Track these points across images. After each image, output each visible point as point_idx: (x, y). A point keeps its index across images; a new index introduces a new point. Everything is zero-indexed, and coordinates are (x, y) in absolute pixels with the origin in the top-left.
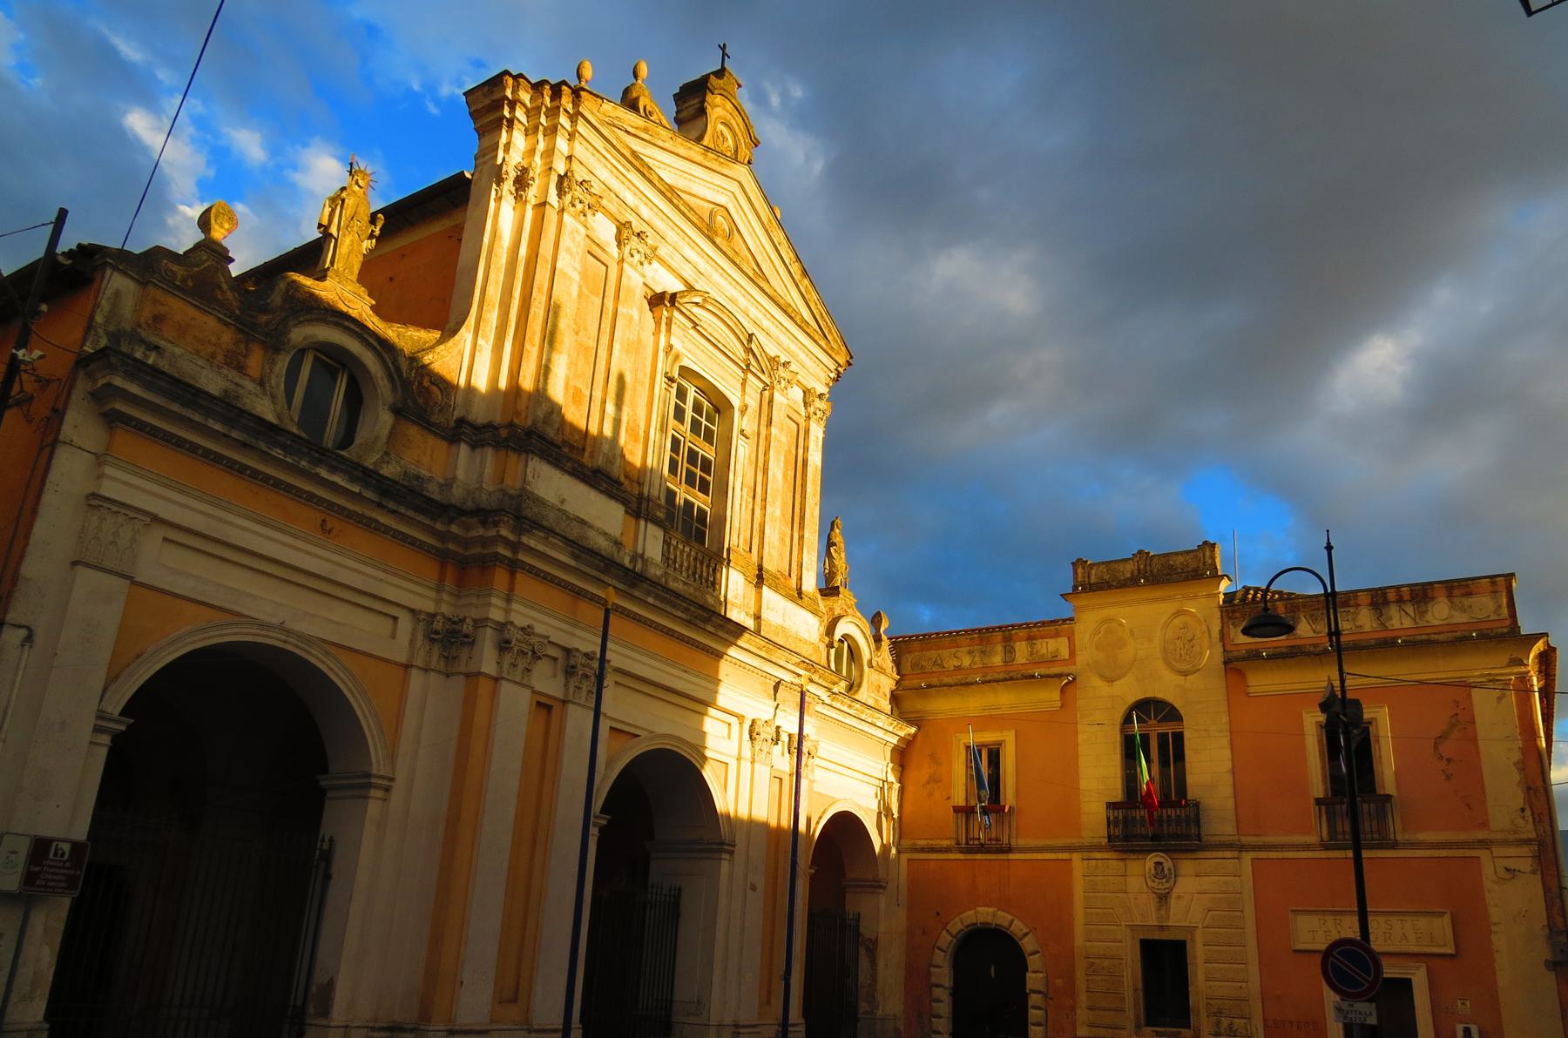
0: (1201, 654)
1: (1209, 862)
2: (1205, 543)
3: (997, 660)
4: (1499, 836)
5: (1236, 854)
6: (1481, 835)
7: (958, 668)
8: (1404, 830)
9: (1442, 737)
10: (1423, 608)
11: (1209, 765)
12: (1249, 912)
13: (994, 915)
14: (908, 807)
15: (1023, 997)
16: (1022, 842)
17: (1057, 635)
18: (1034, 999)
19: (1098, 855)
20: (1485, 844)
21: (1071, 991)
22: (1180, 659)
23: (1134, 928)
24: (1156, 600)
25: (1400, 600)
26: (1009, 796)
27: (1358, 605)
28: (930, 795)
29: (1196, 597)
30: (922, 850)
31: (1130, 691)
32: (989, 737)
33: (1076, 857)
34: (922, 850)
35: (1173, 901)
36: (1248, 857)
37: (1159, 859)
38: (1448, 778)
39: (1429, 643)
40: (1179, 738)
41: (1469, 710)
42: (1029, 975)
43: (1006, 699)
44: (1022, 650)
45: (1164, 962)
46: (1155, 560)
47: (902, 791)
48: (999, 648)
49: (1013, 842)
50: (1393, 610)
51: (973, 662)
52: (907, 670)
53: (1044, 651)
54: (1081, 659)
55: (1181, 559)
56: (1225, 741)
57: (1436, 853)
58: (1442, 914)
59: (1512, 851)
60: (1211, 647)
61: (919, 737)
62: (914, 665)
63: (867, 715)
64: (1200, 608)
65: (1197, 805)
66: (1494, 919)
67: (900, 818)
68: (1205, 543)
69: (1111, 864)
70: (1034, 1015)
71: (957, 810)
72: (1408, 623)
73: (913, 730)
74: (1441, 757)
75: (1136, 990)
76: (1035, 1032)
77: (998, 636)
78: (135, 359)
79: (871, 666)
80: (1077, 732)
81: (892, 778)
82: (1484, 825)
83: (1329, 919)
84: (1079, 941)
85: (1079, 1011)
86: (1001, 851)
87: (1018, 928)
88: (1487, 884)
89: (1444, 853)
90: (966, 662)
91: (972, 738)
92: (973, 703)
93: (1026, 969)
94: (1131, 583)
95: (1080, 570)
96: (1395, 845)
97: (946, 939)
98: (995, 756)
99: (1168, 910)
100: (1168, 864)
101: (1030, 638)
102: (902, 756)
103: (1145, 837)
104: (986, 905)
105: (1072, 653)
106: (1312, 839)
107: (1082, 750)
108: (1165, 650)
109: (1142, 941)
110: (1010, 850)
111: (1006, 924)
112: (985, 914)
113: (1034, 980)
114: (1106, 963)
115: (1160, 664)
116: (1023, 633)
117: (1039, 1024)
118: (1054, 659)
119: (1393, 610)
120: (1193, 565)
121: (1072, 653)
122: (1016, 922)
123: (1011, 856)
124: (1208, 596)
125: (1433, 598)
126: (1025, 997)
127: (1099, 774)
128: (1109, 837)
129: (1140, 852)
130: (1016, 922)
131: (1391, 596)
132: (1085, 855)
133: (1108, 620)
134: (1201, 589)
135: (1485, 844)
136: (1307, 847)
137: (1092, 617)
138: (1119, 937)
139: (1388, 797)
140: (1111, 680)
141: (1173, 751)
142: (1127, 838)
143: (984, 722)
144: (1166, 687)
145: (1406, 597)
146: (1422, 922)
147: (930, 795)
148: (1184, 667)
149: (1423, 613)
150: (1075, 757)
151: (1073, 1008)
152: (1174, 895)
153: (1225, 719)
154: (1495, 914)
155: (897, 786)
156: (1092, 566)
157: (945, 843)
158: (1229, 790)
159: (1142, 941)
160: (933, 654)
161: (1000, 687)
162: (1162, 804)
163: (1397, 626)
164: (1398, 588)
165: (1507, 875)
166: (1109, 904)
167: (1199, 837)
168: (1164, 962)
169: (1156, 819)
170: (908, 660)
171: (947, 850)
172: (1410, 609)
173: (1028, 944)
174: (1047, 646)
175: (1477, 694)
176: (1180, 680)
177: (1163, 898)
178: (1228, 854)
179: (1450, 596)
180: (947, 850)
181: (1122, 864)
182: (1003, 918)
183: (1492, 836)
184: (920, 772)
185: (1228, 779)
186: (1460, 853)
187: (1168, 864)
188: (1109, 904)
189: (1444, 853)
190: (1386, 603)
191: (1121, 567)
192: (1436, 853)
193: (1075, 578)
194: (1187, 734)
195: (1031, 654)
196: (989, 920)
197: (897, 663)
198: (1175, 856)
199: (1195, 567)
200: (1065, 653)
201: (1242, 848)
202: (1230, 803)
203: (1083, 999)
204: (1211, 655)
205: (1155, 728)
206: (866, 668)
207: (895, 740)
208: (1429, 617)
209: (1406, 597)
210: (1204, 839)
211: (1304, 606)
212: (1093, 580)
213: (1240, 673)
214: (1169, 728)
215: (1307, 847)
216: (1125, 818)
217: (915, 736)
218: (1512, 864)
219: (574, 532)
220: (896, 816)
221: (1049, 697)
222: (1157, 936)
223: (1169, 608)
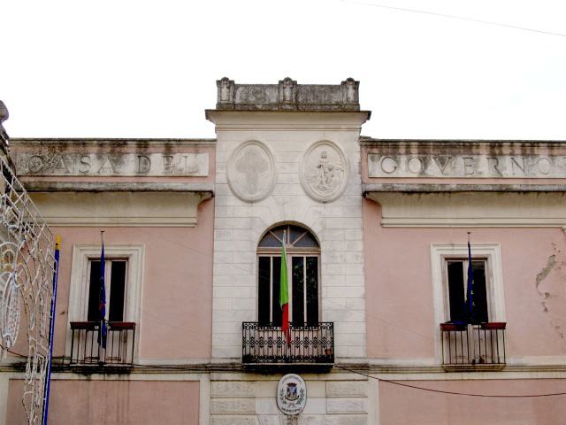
2: (350, 80)
11: (341, 292)
39: (509, 191)
40: (314, 264)
44: (157, 161)
53: (182, 165)
74: (541, 294)
77: (132, 148)
78: (488, 329)
80: (366, 321)
121: (213, 171)
134: (346, 123)
185: (361, 304)
186: (554, 375)
194: (324, 260)
199: (337, 104)
205: (287, 250)
214: (305, 252)
219: (472, 189)
223: (315, 136)
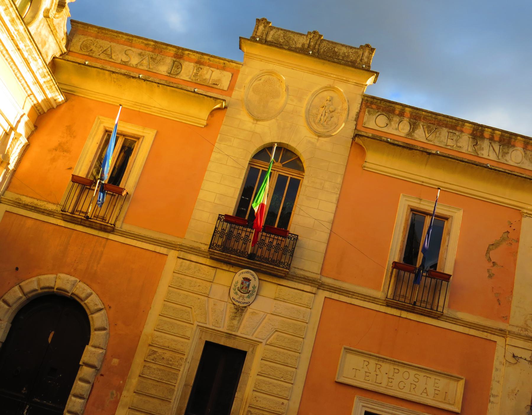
0: (337, 125)
1: (288, 290)
3: (163, 69)
4: (515, 330)
5: (314, 290)
6: (501, 325)
7: (125, 64)
8: (449, 307)
9: (494, 246)
10: (506, 150)
11: (314, 213)
12: (311, 336)
13: (74, 285)
14: (26, 164)
15: (278, 236)
16: (126, 227)
17: (224, 68)
18: (85, 372)
19: (194, 258)
20: (502, 333)
21: (124, 372)
22: (320, 121)
23: (203, 329)
24: (313, 72)
25: (492, 139)
26: (130, 182)
27: (462, 132)
28: (53, 160)
29: (347, 81)
30: (25, 206)
31: (269, 133)
32: (130, 129)
33: (173, 254)
34: (25, 206)
35: (247, 315)
36: (323, 294)
37: (248, 276)
38: (490, 276)
40: (295, 184)
41: (517, 231)
42: (88, 348)
43: (158, 102)
44: (188, 70)
45: (221, 365)
46: (325, 43)
47: (26, 148)
48: (169, 60)
49: (118, 225)
50: (486, 144)
51: (140, 63)
52: (76, 46)
53: (207, 76)
54: (237, 94)
55: (344, 50)
56: (334, 198)
57: (467, 330)
58: (458, 379)
59: (520, 343)
60: (346, 122)
61: (63, 108)
62: (84, 46)
63: (25, 45)
64: (347, 89)
65: (296, 238)
66: (494, 392)
67: (14, 171)
68: (367, 46)
69: (204, 268)
70: (79, 386)
71: (75, 179)
72: (493, 157)
73: (60, 98)
74: (490, 259)
75: (186, 385)
76: (74, 403)
79: (47, 17)
81: (22, 129)
82: (506, 319)
83: (373, 362)
84: (149, 328)
85: (124, 393)
86: (103, 229)
87: (92, 302)
88: (496, 363)
89: (472, 332)
90: (134, 61)
91: (116, 122)
92: (130, 95)
93: (86, 341)
94: (303, 51)
95: (261, 28)
96: (439, 316)
97: (15, 295)
98: (127, 151)
99: (240, 321)
100: (254, 282)
101: (199, 63)
102: (41, 116)
103: (242, 253)
104: (69, 274)
105: (231, 87)
106: (380, 294)
107: (211, 166)
108: (308, 112)
109: (207, 342)
110: (112, 230)
111: (83, 296)
112: (64, 281)
113: (90, 354)
114: (168, 355)
115: (302, 122)
116: (195, 57)
117: (81, 397)
118: (214, 86)
119: (486, 144)
120: (352, 57)
121: (231, 87)
122: (94, 297)
123: (111, 236)
124: (357, 84)
125: (514, 146)
126: (77, 367)
127: (218, 191)
128: (211, 246)
129: (233, 265)
130: (94, 297)
131: (487, 134)
132: (182, 254)
133: (270, 73)
134: (352, 75)
135: (502, 333)
136: (374, 300)
137: (259, 65)
138: (188, 334)
139: (447, 277)
140: (257, 120)
141: (287, 191)
142: (225, 248)
143: (130, 115)
144: (301, 141)
145: (497, 138)
146: (442, 382)
147: (53, 160)
148: (320, 130)
149: (505, 154)
150: (204, 170)
151: (120, 389)
152: (249, 310)
153: (339, 180)
154: (496, 388)
155: (23, 141)
156: (272, 28)
157: (51, 207)
158: (325, 236)
159: (207, 342)
160: (106, 44)
161: (158, 90)
162: (268, 228)
163: (485, 156)
164: (494, 129)
165: (513, 361)
166: (187, 302)
167: (289, 266)
168: (221, 365)
169: (256, 239)
170: (79, 41)
171: (50, 213)
172: (497, 147)
173: (97, 320)
174: (210, 74)
175: (525, 220)
176: (313, 138)
177: (240, 311)
178: (308, 288)
179: (525, 148)
180: (50, 213)
181: (212, 271)
182: (82, 290)
183: (509, 328)
184: (51, 136)
186: (484, 335)
187: (254, 282)
188: (187, 302)
189: (472, 332)
190: (482, 137)
191: (296, 38)
192: (467, 330)
193: (256, 31)
195: (196, 75)
196: (68, 287)
197: (69, 38)
198: (263, 277)
200: (225, 84)
201: (321, 286)
202: (323, 247)
203: (134, 381)
204: (344, 128)
206: (41, 15)
207: (40, 98)
208: (508, 157)
209: (497, 138)
210: (292, 270)
211: (425, 118)
212: (269, 38)
213: (362, 150)
214: (290, 174)
215: (374, 300)
216: (231, 232)
217: (59, 105)
218: (518, 353)
220: (11, 167)
221: (198, 113)
222: (222, 342)
223: (324, 82)
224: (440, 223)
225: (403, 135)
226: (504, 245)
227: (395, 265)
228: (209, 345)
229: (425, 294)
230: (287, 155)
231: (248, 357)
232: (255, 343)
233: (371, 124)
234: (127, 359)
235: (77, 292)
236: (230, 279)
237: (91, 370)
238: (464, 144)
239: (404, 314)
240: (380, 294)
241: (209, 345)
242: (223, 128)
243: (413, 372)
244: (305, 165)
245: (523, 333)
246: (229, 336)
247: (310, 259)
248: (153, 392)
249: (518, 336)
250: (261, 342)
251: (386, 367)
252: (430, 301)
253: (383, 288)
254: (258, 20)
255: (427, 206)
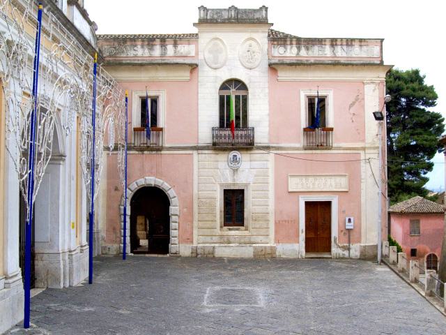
1: (257, 154)
31: (225, 76)
37: (235, 154)
40: (245, 99)
49: (164, 145)
53: (182, 51)
68: (264, 6)
82: (364, 141)
83: (304, 179)
106: (298, 145)
113: (173, 209)
114: (208, 201)
117: (175, 229)
121: (197, 53)
139: (332, 129)
141: (243, 102)
146: (338, 179)
151: (192, 222)
172: (345, 47)
189: (348, 152)
192: (346, 152)
203: (196, 216)
214: (241, 93)
224: (322, 100)
225: (294, 55)
226: (357, 103)
227: (305, 130)
228: (226, 191)
229: (142, 139)
230: (239, 84)
231: (245, 192)
232: (247, 185)
233: (276, 54)
234: (191, 209)
235: (156, 184)
236: (223, 159)
237: (177, 217)
238: (327, 52)
239: (314, 152)
240: (302, 146)
241: (226, 191)
242: (200, 79)
243: (323, 178)
244: (248, 86)
245: (373, 146)
246: (234, 184)
247: (261, 137)
248: (207, 219)
249: (370, 148)
250: (254, 183)
251: (311, 179)
252: (325, 141)
253: (301, 141)
254: (199, 8)
255: (314, 93)
